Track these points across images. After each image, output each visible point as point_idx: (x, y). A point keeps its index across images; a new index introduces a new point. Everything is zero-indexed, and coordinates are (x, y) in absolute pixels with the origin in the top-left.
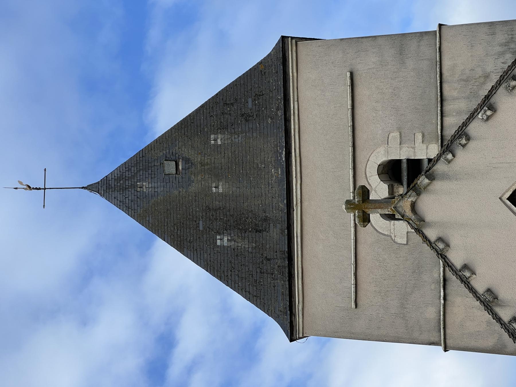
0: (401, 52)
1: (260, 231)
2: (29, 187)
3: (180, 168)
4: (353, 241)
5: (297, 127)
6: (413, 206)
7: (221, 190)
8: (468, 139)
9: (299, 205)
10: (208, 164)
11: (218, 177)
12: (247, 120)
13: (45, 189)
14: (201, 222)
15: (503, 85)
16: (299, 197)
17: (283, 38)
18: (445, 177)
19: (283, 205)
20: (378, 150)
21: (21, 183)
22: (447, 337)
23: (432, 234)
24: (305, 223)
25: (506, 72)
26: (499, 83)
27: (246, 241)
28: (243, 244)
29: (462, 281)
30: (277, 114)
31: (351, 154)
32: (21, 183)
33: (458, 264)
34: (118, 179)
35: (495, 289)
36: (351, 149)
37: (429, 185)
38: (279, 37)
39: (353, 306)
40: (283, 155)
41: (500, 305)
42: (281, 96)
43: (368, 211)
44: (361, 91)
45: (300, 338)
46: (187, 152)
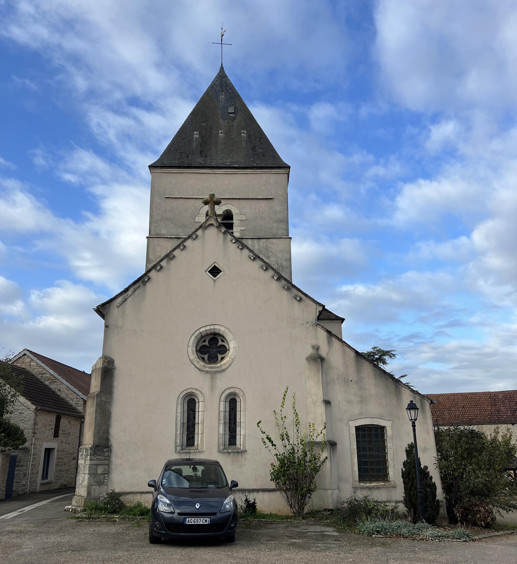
0: (281, 221)
1: (201, 153)
4: (196, 197)
6: (212, 225)
12: (252, 149)
18: (225, 239)
19: (213, 164)
21: (225, 31)
23: (199, 233)
26: (265, 262)
28: (195, 144)
29: (178, 245)
32: (225, 31)
34: (226, 83)
36: (238, 197)
37: (221, 232)
38: (290, 165)
39: (166, 196)
40: (236, 166)
41: (168, 261)
42: (263, 165)
43: (210, 204)
44: (264, 203)
46: (238, 119)
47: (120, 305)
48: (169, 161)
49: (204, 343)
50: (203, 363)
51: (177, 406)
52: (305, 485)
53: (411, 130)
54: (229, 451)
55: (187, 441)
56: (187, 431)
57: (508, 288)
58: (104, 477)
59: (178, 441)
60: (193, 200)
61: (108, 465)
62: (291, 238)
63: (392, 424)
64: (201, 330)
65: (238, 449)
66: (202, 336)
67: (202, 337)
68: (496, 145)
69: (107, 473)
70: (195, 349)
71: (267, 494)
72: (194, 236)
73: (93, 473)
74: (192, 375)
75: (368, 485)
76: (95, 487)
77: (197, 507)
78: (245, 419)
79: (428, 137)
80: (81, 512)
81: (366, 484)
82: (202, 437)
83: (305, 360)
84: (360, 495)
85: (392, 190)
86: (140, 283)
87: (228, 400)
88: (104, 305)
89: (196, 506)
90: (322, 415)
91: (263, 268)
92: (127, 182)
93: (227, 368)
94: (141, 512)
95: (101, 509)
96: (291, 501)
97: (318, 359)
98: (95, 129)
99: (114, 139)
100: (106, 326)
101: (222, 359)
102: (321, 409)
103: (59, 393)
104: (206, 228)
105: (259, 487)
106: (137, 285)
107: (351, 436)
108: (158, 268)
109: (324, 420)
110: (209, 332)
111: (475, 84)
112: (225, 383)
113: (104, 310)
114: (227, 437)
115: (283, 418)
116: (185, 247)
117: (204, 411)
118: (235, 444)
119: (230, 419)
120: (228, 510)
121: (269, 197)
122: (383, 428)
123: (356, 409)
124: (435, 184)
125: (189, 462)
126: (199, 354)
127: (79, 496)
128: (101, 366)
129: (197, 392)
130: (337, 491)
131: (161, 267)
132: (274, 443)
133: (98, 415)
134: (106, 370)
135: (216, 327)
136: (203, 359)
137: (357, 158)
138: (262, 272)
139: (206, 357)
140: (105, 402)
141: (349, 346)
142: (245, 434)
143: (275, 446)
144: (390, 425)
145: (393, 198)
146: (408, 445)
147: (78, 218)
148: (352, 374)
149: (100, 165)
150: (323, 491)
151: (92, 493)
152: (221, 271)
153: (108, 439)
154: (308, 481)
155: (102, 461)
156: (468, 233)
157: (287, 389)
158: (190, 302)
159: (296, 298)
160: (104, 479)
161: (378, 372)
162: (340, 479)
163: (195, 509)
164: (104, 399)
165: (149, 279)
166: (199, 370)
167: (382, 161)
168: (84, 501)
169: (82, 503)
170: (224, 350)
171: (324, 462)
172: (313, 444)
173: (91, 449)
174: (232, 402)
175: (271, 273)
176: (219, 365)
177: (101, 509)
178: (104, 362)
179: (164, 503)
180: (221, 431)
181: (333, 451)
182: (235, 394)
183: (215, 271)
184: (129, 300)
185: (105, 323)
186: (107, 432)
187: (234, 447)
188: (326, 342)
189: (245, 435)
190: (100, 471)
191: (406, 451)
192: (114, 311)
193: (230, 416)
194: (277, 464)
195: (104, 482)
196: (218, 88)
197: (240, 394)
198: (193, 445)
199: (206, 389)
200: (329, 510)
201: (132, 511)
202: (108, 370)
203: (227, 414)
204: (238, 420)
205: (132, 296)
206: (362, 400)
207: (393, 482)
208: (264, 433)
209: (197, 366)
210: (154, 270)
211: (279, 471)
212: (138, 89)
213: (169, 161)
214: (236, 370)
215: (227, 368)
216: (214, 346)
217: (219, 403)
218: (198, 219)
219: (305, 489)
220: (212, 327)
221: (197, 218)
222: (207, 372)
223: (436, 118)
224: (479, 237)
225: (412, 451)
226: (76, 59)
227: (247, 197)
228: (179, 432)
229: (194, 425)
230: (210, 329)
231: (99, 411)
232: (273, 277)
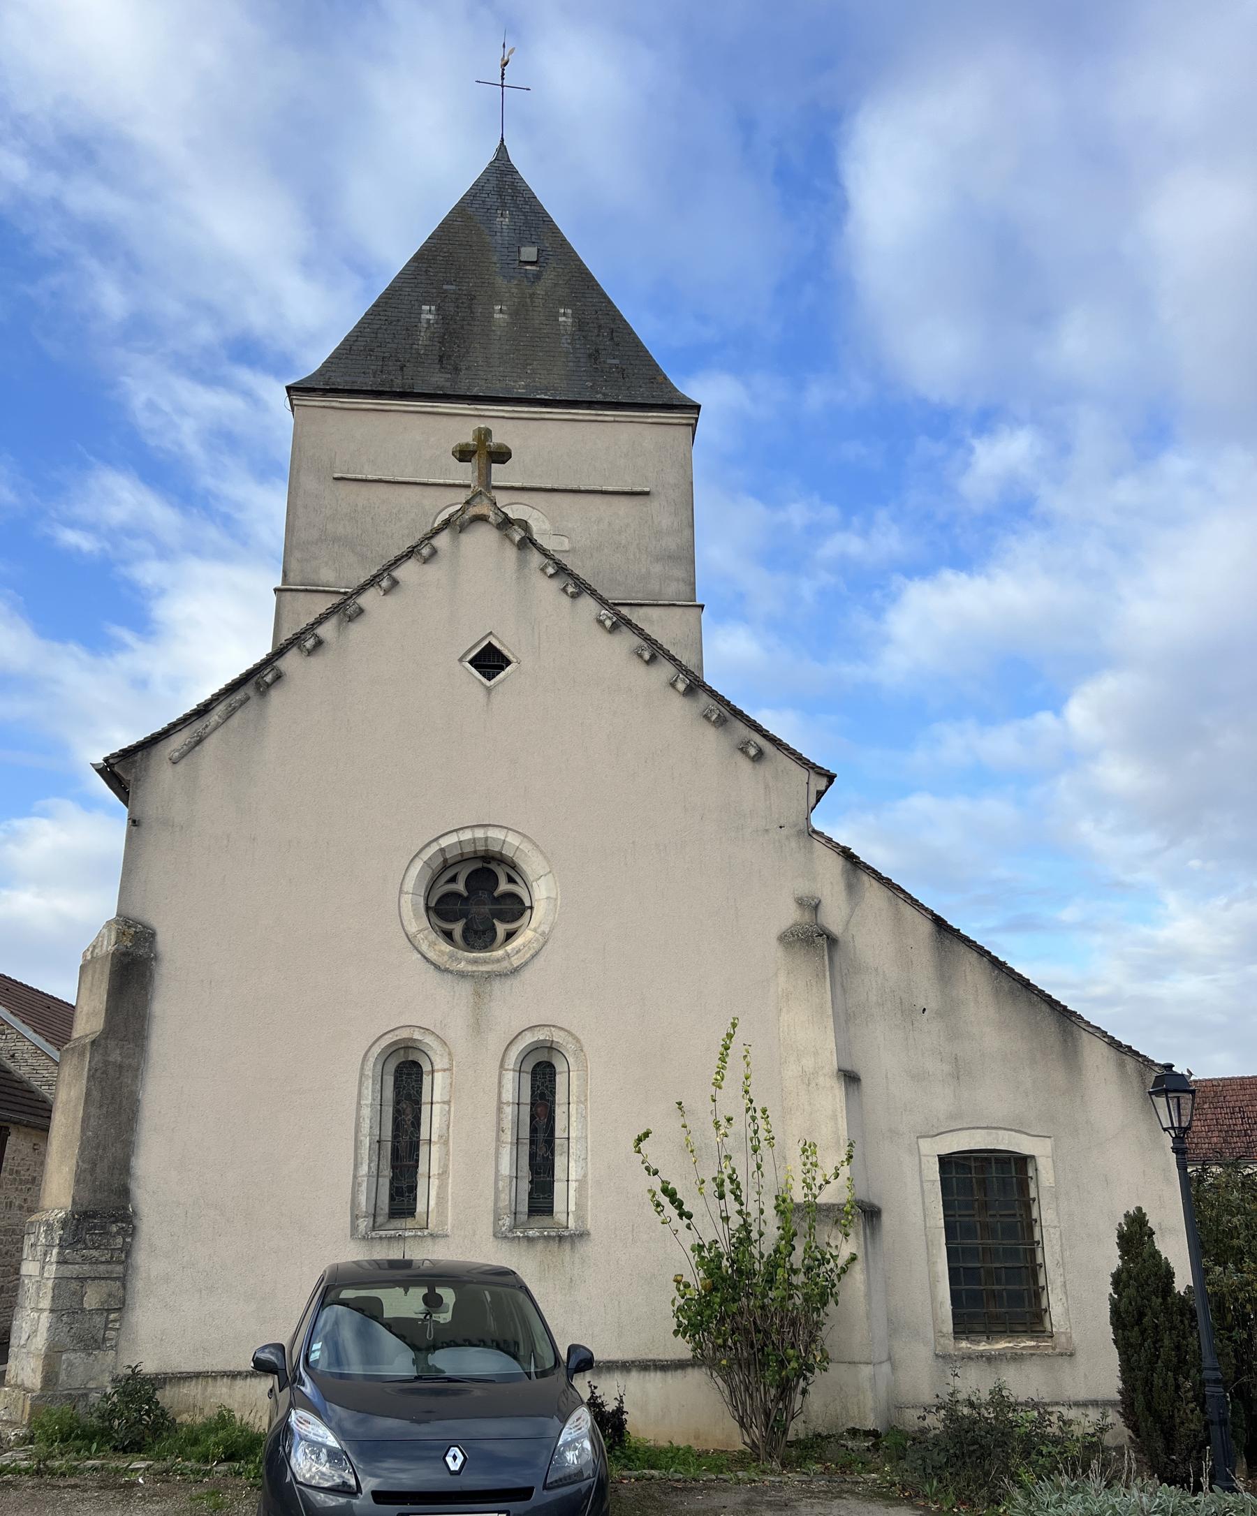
0: (671, 558)
1: (441, 361)
2: (506, 64)
4: (425, 480)
5: (580, 417)
6: (482, 518)
7: (497, 316)
8: (574, 596)
10: (532, 302)
12: (590, 356)
15: (643, 643)
17: (698, 407)
18: (522, 564)
19: (475, 391)
20: (547, 522)
21: (511, 53)
23: (442, 541)
25: (661, 647)
26: (647, 638)
27: (428, 343)
28: (423, 337)
29: (375, 577)
30: (597, 393)
31: (543, 486)
32: (511, 53)
33: (398, 573)
34: (513, 186)
35: (363, 619)
36: (549, 486)
37: (512, 541)
38: (699, 402)
39: (336, 475)
40: (543, 396)
41: (340, 623)
42: (621, 399)
43: (475, 460)
44: (623, 504)
45: (291, 401)
46: (549, 277)
47: (183, 756)
48: (347, 378)
49: (452, 887)
50: (446, 948)
51: (361, 1084)
52: (791, 1352)
53: (926, 447)
54: (531, 1233)
55: (392, 1198)
56: (393, 1167)
57: (1147, 841)
58: (107, 1322)
59: (363, 1199)
60: (417, 489)
61: (123, 1280)
62: (702, 607)
63: (1055, 1148)
64: (444, 842)
66: (445, 860)
67: (446, 867)
68: (1127, 491)
69: (118, 1306)
70: (422, 901)
71: (656, 1378)
72: (425, 551)
73: (67, 1308)
74: (416, 986)
75: (983, 1347)
76: (72, 1356)
77: (454, 1466)
78: (585, 1127)
79: (967, 465)
80: (18, 1444)
82: (442, 1187)
83: (774, 942)
84: (974, 1383)
85: (877, 594)
86: (249, 690)
87: (528, 1067)
88: (127, 754)
89: (449, 1459)
90: (834, 1117)
91: (640, 656)
92: (221, 556)
93: (526, 964)
94: (226, 1447)
95: (88, 1436)
96: (743, 1404)
97: (815, 940)
98: (143, 419)
99: (193, 448)
100: (134, 822)
101: (510, 935)
102: (833, 1096)
103: (10, 1065)
104: (462, 529)
105: (629, 1356)
106: (239, 696)
107: (927, 1186)
108: (309, 644)
109: (844, 1133)
110: (468, 849)
111: (1081, 344)
112: (518, 1011)
113: (127, 770)
114: (525, 1186)
115: (723, 1122)
116: (395, 583)
117: (448, 1103)
118: (549, 1211)
119: (534, 1130)
120: (572, 1470)
121: (638, 489)
122: (1022, 1162)
123: (941, 1101)
124: (979, 583)
125: (402, 1274)
126: (434, 919)
127: (17, 1386)
128: (111, 949)
129: (428, 1039)
130: (886, 1368)
131: (319, 643)
132: (686, 1208)
133: (93, 1111)
134: (128, 959)
135: (492, 833)
136: (448, 935)
137: (797, 514)
138: (639, 669)
139: (458, 928)
140: (121, 1066)
141: (914, 903)
142: (585, 1176)
143: (689, 1216)
145: (877, 613)
146: (1127, 1215)
147: (98, 644)
148: (925, 988)
149: (160, 514)
150: (843, 1367)
151: (63, 1377)
152: (508, 663)
153: (124, 1193)
154: (803, 1336)
155: (102, 1268)
156: (1056, 703)
157: (734, 1025)
158: (406, 758)
159: (743, 751)
160: (106, 1328)
161: (1006, 984)
162: (894, 1327)
163: (448, 1476)
164: (115, 1056)
165: (279, 677)
166: (437, 967)
167: (856, 521)
168: (32, 1406)
169: (23, 1412)
170: (515, 908)
171: (844, 1271)
172: (814, 1212)
173: (64, 1224)
174: (542, 1075)
175: (665, 670)
176: (500, 953)
177: (88, 1436)
178: (121, 934)
179: (316, 1446)
180: (506, 1167)
181: (873, 1234)
182: (550, 1047)
183: (490, 661)
185: (130, 813)
186: (123, 1168)
187: (545, 1220)
189: (582, 1182)
190: (92, 1299)
191: (1121, 1236)
192: (163, 777)
193: (532, 1118)
194: (696, 1279)
195: (104, 1340)
196: (492, 200)
197: (569, 1047)
198: (411, 1212)
200: (868, 1434)
201: (195, 1442)
202: (131, 964)
203: (526, 1110)
204: (559, 1132)
205: (220, 730)
206: (959, 1072)
207: (1063, 1339)
208: (656, 1173)
209: (431, 955)
210: (295, 650)
211: (704, 1302)
212: (256, 318)
213: (347, 378)
214: (554, 968)
215: (526, 964)
216: (484, 895)
217: (500, 1076)
219: (794, 1364)
220: (480, 833)
222: (462, 975)
223: (987, 420)
224: (1080, 714)
225: (1135, 1235)
226: (101, 239)
227: (575, 487)
228: (364, 1169)
229: (414, 1147)
230: (474, 840)
231: (96, 1094)
232: (673, 685)
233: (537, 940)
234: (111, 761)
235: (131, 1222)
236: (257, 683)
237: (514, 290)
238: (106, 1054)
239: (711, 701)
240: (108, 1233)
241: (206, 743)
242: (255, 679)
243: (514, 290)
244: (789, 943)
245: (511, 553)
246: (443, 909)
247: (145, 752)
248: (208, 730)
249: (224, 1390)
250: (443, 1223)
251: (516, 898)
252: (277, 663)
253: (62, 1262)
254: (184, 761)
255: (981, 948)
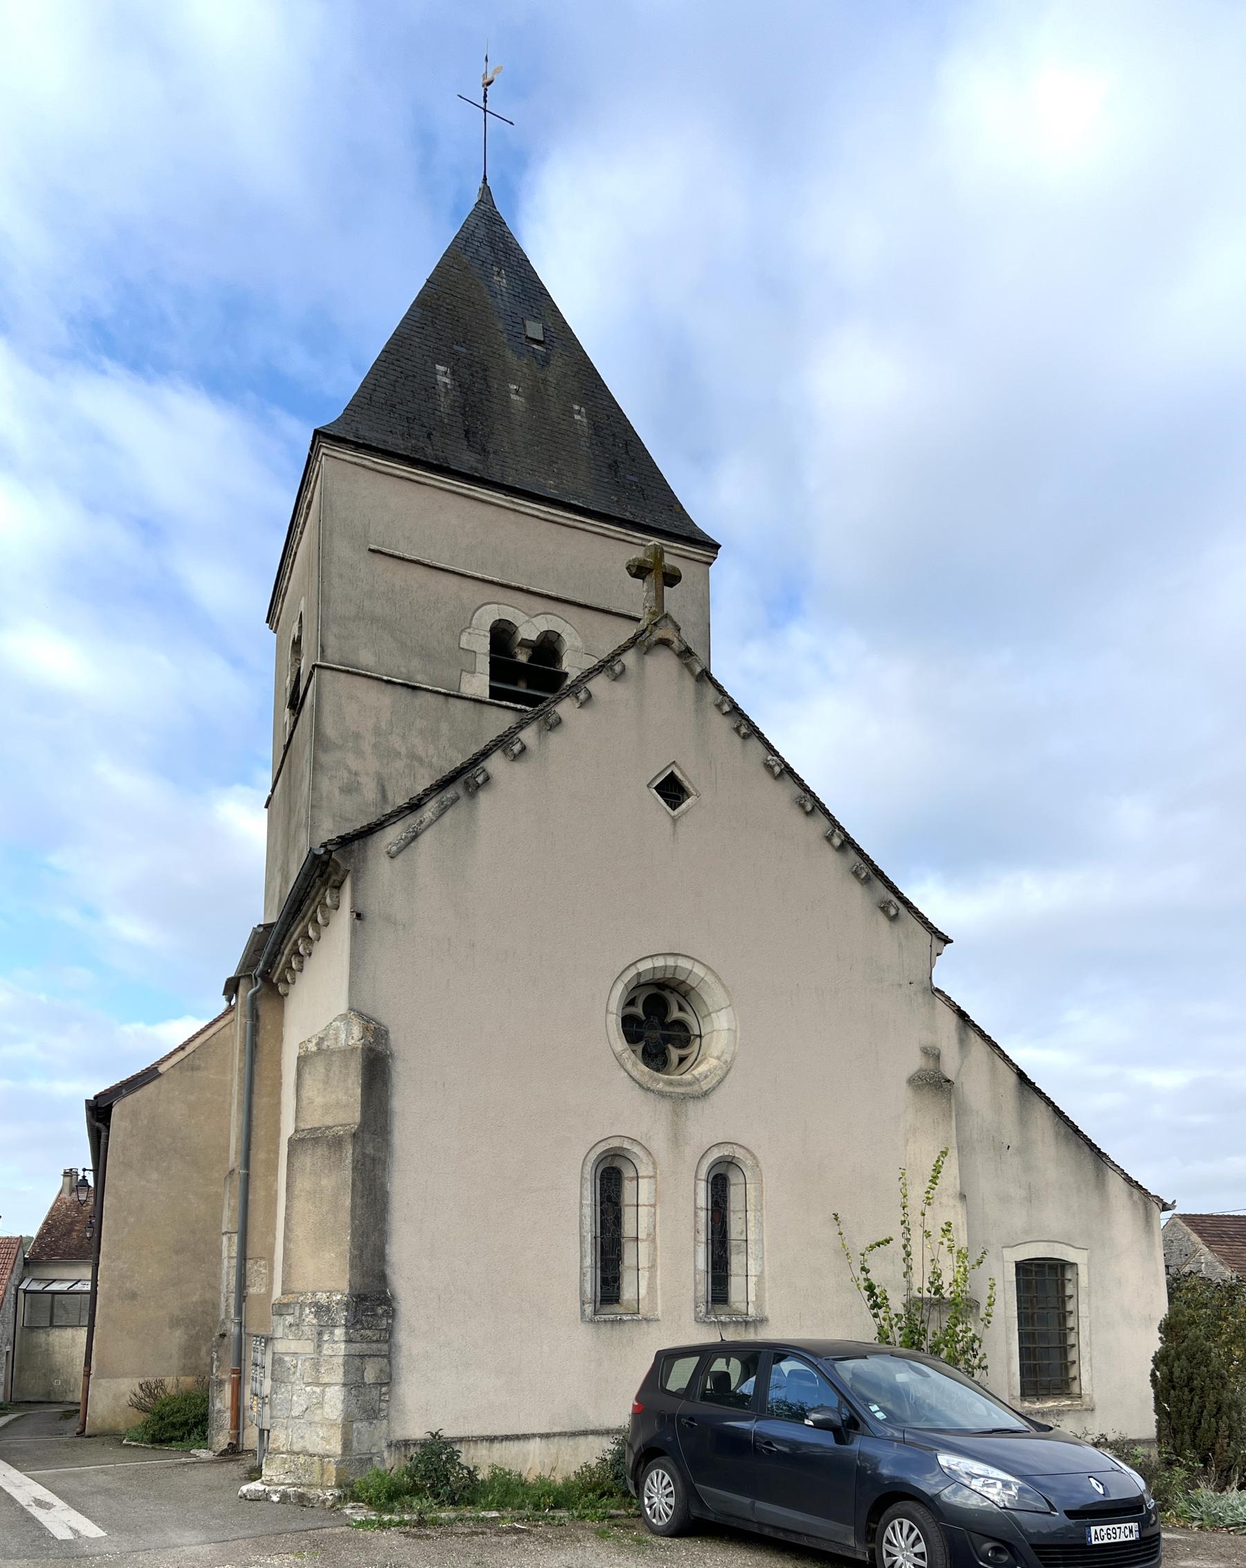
2: (489, 83)
3: (535, 346)
5: (611, 534)
6: (665, 643)
8: (745, 737)
9: (512, 506)
11: (530, 398)
12: (610, 466)
13: (485, 111)
14: (464, 350)
16: (522, 509)
17: (718, 546)
18: (699, 697)
19: (509, 481)
21: (495, 72)
22: (335, 673)
23: (629, 658)
24: (480, 505)
28: (444, 404)
36: (582, 601)
39: (373, 547)
41: (540, 731)
43: (650, 578)
46: (556, 362)
47: (400, 851)
48: (375, 434)
61: (389, 1357)
63: (1089, 1259)
65: (738, 1313)
69: (387, 1381)
74: (614, 1097)
81: (1034, 1403)
82: (652, 1279)
83: (904, 1084)
93: (713, 1089)
97: (934, 1083)
106: (449, 793)
107: (1007, 1285)
112: (709, 1128)
117: (654, 1206)
129: (636, 1149)
133: (358, 1201)
135: (682, 963)
141: (1006, 1058)
142: (762, 1272)
144: (1086, 1261)
148: (1010, 1134)
151: (355, 1444)
153: (383, 1278)
155: (374, 1346)
161: (1064, 1129)
164: (370, 1150)
166: (641, 1086)
168: (337, 1469)
183: (672, 790)
184: (426, 839)
186: (380, 1255)
188: (954, 1041)
189: (760, 1277)
195: (380, 1410)
199: (659, 1144)
205: (434, 828)
206: (1032, 1197)
207: (1087, 1399)
209: (635, 1074)
215: (713, 1089)
218: (468, 642)
220: (671, 962)
221: (464, 637)
222: (662, 1094)
233: (721, 1068)
234: (329, 847)
235: (390, 1306)
236: (466, 783)
237: (525, 370)
238: (363, 1147)
239: (859, 859)
240: (376, 1315)
241: (422, 839)
242: (465, 777)
243: (525, 370)
244: (918, 1086)
245: (689, 683)
246: (632, 1028)
247: (361, 841)
248: (423, 826)
249: (484, 1452)
250: (654, 1309)
251: (682, 1025)
252: (483, 764)
253: (349, 1341)
254: (401, 857)
255: (1048, 1099)
